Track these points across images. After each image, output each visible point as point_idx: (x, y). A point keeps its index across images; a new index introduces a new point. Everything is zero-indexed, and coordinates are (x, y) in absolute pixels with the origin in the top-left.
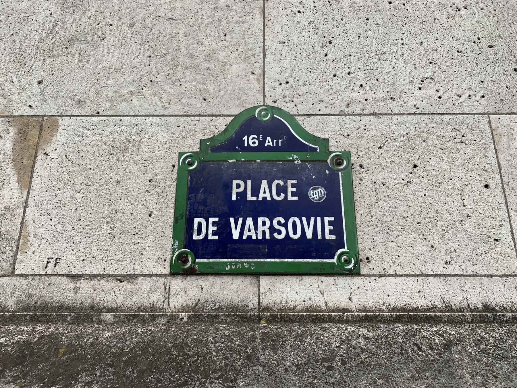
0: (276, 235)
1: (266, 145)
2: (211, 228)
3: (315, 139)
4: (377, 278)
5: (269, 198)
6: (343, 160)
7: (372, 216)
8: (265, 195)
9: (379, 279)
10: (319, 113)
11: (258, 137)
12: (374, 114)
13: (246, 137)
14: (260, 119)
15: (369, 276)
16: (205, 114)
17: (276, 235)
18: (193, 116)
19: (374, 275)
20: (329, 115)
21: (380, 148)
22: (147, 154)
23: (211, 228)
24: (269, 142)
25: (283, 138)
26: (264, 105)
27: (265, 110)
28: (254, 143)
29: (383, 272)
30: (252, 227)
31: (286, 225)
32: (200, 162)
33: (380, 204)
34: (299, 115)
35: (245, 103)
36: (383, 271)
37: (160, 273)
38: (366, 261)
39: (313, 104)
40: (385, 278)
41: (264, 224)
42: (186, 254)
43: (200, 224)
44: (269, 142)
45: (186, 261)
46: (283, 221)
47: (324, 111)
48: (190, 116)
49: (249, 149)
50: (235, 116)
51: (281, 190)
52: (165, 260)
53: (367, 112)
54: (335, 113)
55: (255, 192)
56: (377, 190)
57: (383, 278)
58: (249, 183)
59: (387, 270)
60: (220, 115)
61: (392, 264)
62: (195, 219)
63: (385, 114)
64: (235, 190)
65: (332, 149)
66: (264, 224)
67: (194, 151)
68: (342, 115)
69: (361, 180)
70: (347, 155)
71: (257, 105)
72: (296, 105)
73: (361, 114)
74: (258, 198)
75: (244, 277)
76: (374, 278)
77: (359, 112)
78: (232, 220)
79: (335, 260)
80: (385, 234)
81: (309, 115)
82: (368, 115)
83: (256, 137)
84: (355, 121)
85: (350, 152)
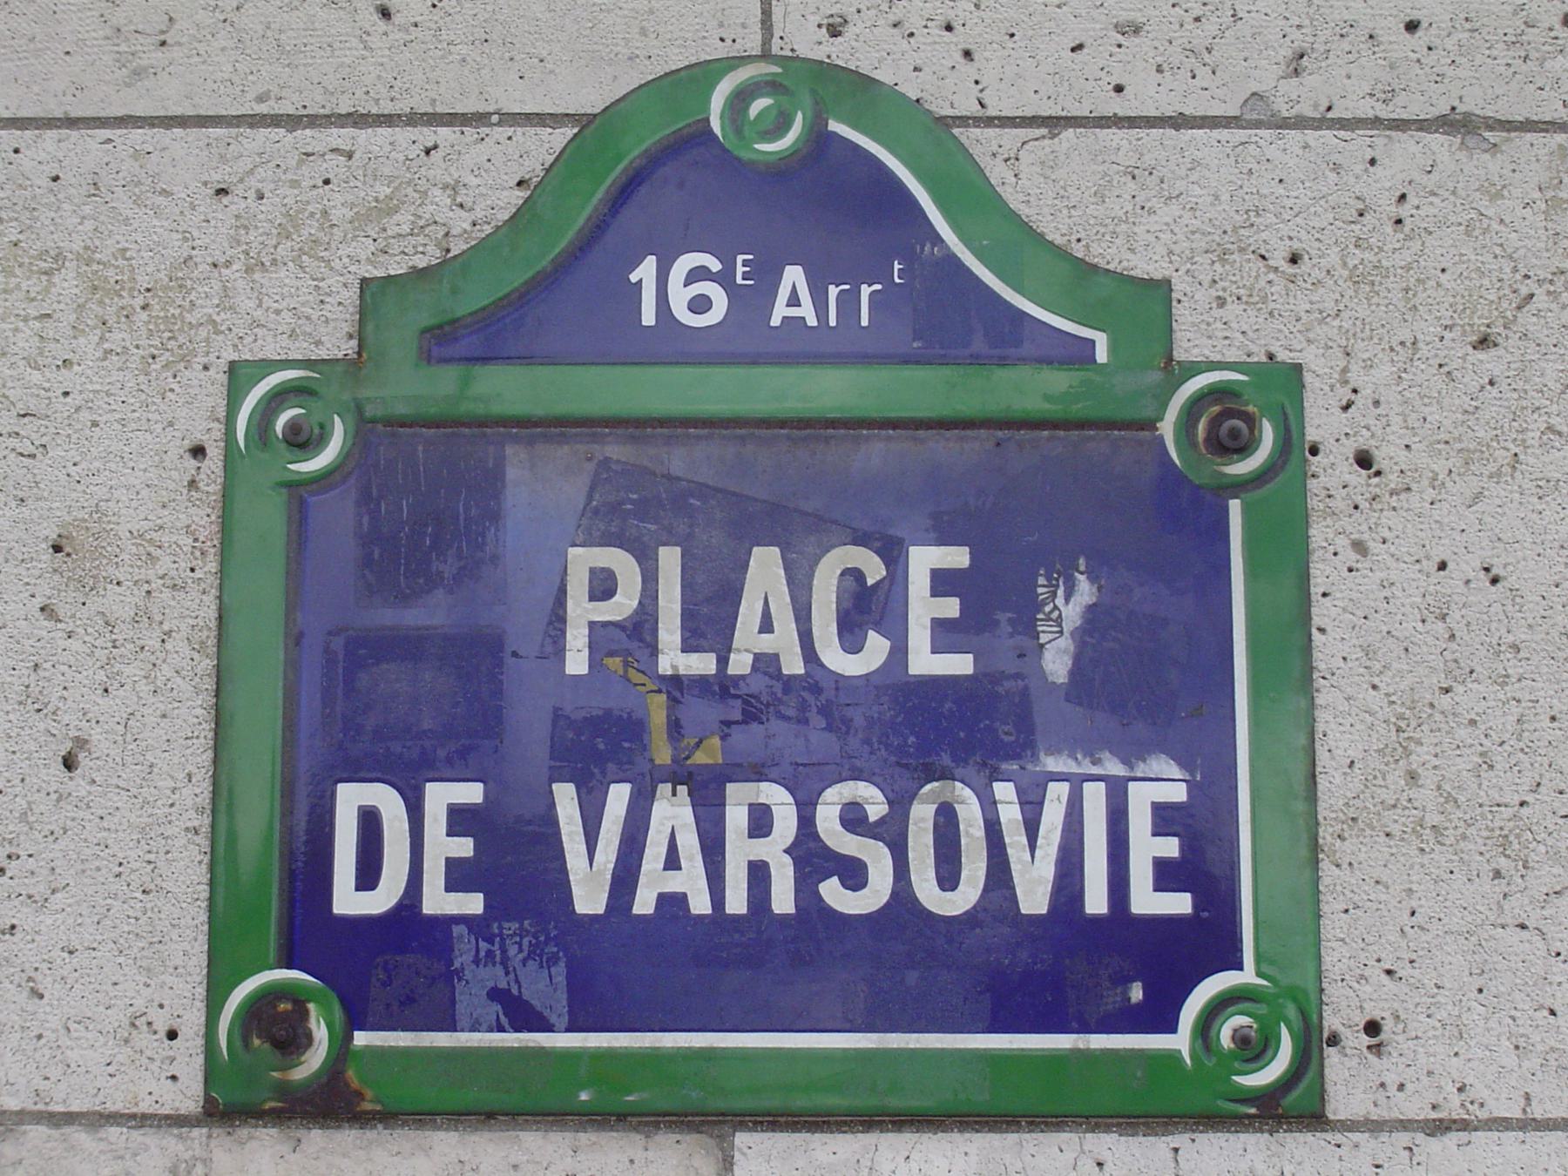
0: (832, 892)
1: (776, 321)
2: (444, 846)
3: (1081, 280)
4: (1420, 1137)
5: (794, 665)
6: (1250, 420)
7: (1412, 776)
8: (766, 643)
9: (1433, 1147)
10: (1119, 106)
11: (729, 268)
12: (1456, 124)
13: (650, 263)
14: (730, 143)
15: (1374, 1126)
16: (387, 108)
17: (832, 892)
18: (314, 121)
19: (1405, 1125)
20: (1179, 122)
21: (1484, 342)
22: (36, 376)
23: (444, 846)
24: (794, 301)
25: (885, 276)
26: (766, 56)
27: (772, 86)
28: (700, 305)
29: (1453, 1108)
30: (689, 843)
31: (893, 835)
32: (365, 430)
33: (1466, 698)
34: (989, 122)
35: (643, 32)
36: (1456, 1099)
37: (145, 1107)
38: (1366, 1040)
39: (1078, 48)
40: (1463, 1136)
41: (760, 822)
42: (299, 1000)
43: (370, 821)
44: (794, 301)
45: (292, 1041)
46: (877, 809)
47: (1146, 98)
48: (292, 122)
49: (672, 344)
50: (585, 122)
51: (866, 609)
52: (172, 1035)
53: (1416, 108)
54: (1217, 110)
55: (710, 621)
56: (1455, 615)
57: (1453, 1138)
58: (670, 559)
59: (1479, 1091)
60: (480, 119)
61: (1510, 1060)
62: (342, 788)
63: (1528, 126)
64: (581, 612)
65: (1187, 347)
66: (760, 822)
67: (323, 354)
68: (1258, 124)
69: (1359, 547)
70: (1284, 381)
71: (721, 51)
72: (967, 54)
73: (1376, 122)
74: (723, 661)
75: (638, 1138)
76: (1404, 1138)
77: (1367, 109)
78: (565, 797)
79: (1180, 1041)
80: (1486, 885)
81: (1055, 124)
82: (1422, 125)
83: (715, 265)
84: (1336, 168)
85: (1298, 368)
